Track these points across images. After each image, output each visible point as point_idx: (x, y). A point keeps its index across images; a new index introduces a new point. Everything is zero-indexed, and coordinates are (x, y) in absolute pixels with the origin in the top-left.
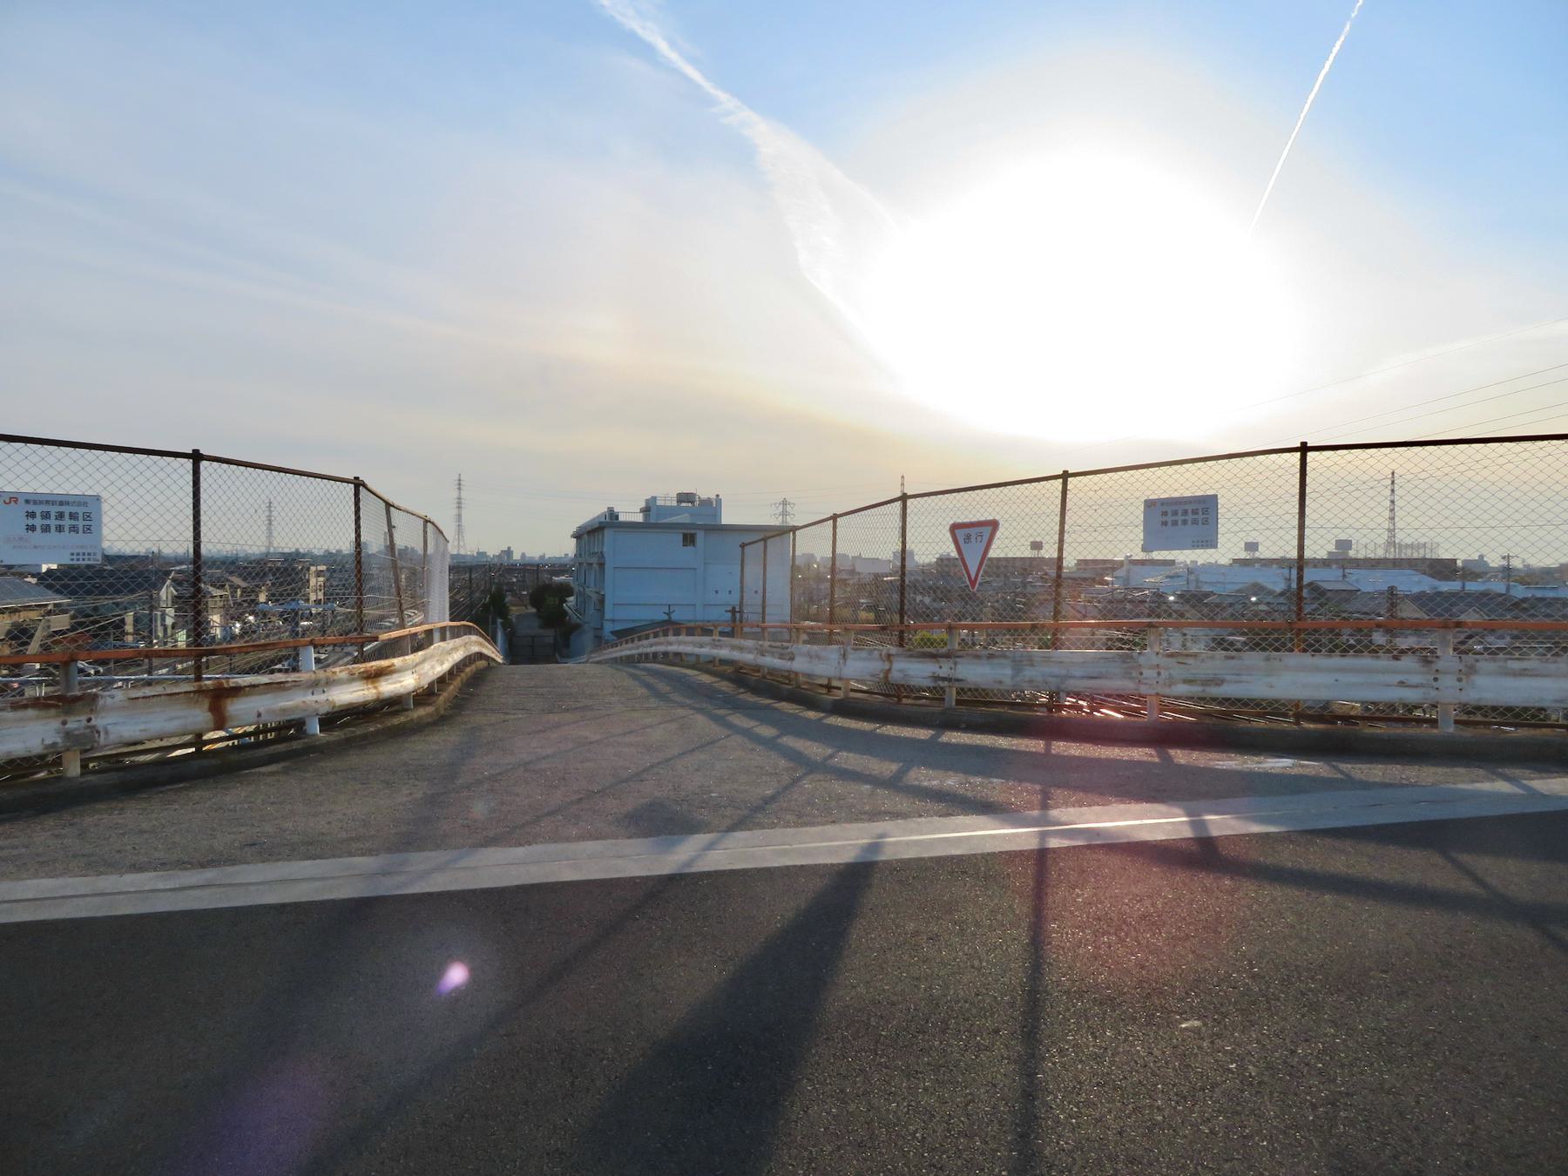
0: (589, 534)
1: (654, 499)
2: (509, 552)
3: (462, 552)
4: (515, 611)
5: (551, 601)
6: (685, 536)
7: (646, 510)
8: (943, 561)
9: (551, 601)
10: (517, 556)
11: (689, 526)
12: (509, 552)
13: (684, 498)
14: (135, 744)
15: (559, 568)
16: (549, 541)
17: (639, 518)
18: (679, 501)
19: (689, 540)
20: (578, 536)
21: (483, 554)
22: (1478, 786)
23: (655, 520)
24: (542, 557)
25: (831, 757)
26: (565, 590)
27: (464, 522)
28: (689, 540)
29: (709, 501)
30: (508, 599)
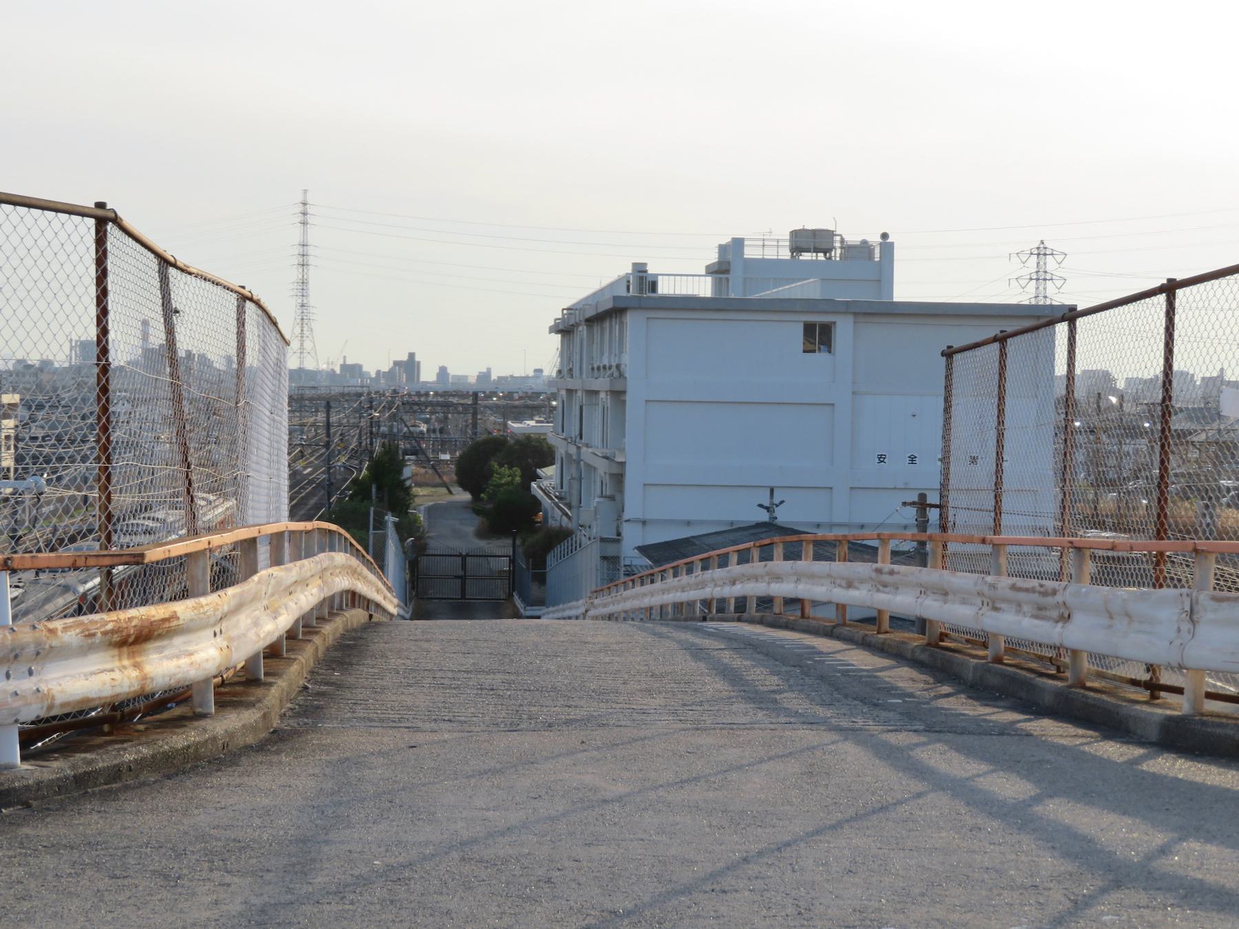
0: (593, 324)
1: (738, 243)
2: (410, 365)
3: (310, 365)
4: (424, 498)
5: (505, 475)
6: (809, 329)
7: (720, 271)
9: (505, 475)
10: (428, 375)
11: (821, 303)
12: (410, 365)
13: (808, 241)
15: (524, 400)
18: (796, 249)
19: (818, 336)
20: (565, 329)
21: (352, 370)
26: (534, 454)
27: (312, 300)
28: (818, 336)
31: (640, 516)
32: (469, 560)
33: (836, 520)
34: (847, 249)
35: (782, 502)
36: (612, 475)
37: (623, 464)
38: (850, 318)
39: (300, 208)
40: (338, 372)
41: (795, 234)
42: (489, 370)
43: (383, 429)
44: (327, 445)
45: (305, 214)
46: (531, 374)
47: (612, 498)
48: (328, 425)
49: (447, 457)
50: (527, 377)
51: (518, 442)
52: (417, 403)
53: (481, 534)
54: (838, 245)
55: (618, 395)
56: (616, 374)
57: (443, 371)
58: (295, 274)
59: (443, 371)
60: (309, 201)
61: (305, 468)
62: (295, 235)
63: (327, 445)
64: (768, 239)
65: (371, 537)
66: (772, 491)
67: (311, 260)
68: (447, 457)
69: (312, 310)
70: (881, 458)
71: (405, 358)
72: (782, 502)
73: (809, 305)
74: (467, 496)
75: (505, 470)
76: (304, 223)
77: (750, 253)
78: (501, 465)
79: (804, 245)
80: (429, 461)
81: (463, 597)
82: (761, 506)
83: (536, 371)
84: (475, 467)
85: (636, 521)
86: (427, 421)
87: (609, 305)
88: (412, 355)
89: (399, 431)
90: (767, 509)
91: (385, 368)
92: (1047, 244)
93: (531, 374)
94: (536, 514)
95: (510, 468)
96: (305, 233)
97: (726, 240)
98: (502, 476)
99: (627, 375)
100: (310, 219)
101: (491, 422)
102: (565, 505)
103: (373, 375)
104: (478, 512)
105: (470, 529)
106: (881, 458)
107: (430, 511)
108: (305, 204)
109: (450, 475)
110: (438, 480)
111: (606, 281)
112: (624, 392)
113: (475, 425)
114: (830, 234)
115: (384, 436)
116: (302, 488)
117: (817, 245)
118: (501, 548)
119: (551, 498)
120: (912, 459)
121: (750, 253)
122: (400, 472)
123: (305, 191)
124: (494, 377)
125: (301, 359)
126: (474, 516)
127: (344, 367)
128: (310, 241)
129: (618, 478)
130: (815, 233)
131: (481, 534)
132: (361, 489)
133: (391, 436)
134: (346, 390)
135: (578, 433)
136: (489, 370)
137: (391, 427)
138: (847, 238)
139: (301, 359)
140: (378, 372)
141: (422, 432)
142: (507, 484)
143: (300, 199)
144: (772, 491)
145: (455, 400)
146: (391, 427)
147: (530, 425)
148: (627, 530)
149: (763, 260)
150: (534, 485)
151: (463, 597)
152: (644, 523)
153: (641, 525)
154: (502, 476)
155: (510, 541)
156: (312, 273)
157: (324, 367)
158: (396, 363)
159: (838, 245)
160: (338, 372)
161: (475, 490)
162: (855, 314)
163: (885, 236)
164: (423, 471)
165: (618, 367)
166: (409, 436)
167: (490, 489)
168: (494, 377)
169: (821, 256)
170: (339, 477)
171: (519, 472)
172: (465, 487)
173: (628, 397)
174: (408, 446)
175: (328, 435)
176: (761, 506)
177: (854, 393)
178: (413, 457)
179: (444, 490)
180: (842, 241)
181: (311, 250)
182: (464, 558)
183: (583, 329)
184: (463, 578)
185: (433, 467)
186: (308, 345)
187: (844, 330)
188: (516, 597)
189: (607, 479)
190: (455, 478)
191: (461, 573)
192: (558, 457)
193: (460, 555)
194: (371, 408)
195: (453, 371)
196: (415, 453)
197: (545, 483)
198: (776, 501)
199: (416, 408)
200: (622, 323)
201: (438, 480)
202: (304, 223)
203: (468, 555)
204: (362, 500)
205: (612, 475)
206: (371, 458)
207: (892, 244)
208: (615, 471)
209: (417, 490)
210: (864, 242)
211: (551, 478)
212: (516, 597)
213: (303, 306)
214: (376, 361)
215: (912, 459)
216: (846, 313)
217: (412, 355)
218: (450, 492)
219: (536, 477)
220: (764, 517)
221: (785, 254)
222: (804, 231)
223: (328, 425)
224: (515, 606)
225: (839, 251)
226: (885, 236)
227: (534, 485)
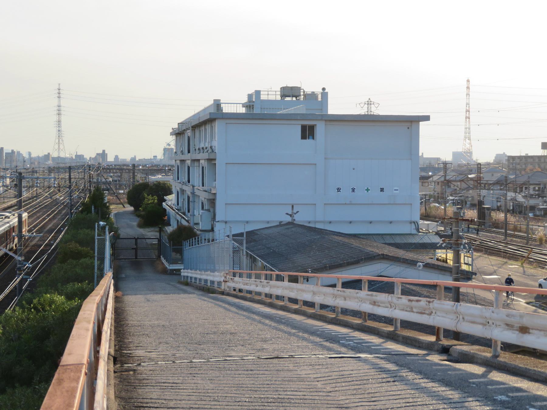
0: (191, 131)
1: (258, 93)
2: (103, 155)
3: (62, 155)
4: (115, 209)
5: (150, 199)
6: (304, 128)
7: (249, 105)
8: (161, 160)
9: (150, 199)
10: (111, 159)
11: (301, 117)
12: (103, 155)
13: (289, 92)
14: (279, 320)
15: (154, 168)
16: (141, 139)
17: (243, 110)
18: (283, 96)
19: (308, 132)
20: (179, 133)
21: (80, 157)
22: (75, 405)
23: (257, 112)
24: (134, 159)
25: (383, 343)
26: (163, 190)
27: (63, 128)
28: (308, 132)
29: (313, 95)
30: (107, 198)
31: (224, 220)
32: (139, 241)
33: (317, 220)
34: (305, 95)
35: (298, 212)
36: (209, 200)
37: (215, 194)
38: (324, 123)
39: (58, 91)
40: (74, 158)
41: (283, 89)
42: (135, 156)
43: (95, 180)
44: (70, 187)
45: (59, 93)
46: (152, 158)
47: (208, 210)
48: (70, 178)
49: (122, 192)
50: (151, 159)
51: (154, 185)
52: (109, 169)
53: (140, 226)
54: (302, 93)
55: (211, 161)
56: (210, 151)
57: (117, 157)
58: (56, 118)
59: (117, 157)
60: (61, 88)
61: (61, 196)
62: (56, 102)
63: (70, 187)
64: (271, 92)
65: (96, 240)
66: (293, 206)
67: (62, 112)
68: (122, 192)
69: (63, 133)
70: (339, 190)
71: (101, 152)
72: (298, 212)
73: (303, 117)
74: (132, 209)
75: (150, 197)
76: (59, 97)
77: (263, 97)
78: (148, 195)
79: (288, 94)
80: (114, 193)
81: (136, 258)
82: (287, 214)
83: (154, 156)
84: (136, 195)
85: (222, 221)
86: (111, 177)
87: (208, 117)
88: (104, 151)
89: (101, 180)
90: (291, 215)
91: (93, 156)
92: (371, 100)
93: (152, 158)
94: (165, 217)
95: (152, 196)
96: (60, 101)
97: (251, 91)
98: (149, 200)
99: (216, 151)
100: (61, 96)
101: (140, 178)
102: (181, 213)
103: (88, 159)
104: (138, 216)
105: (135, 224)
106: (339, 190)
107: (116, 215)
108: (59, 89)
109: (125, 199)
110: (119, 202)
111: (197, 112)
112: (215, 160)
113: (134, 178)
114: (299, 89)
115: (94, 183)
116: (60, 206)
117: (294, 94)
118: (151, 234)
119: (174, 210)
120: (353, 190)
121: (263, 97)
122: (103, 199)
123: (59, 84)
124: (137, 159)
125: (59, 152)
126: (137, 218)
127: (76, 156)
128: (62, 104)
129: (212, 202)
130: (292, 88)
131: (140, 226)
132: (86, 208)
133: (98, 183)
134: (78, 164)
135: (187, 179)
136: (135, 156)
137: (98, 179)
138: (306, 90)
139: (59, 152)
140: (90, 158)
141: (110, 181)
142: (151, 203)
143: (58, 87)
144: (293, 206)
145: (125, 167)
146: (98, 179)
147: (159, 177)
148: (218, 227)
149: (268, 100)
150: (164, 204)
151: (136, 258)
152: (226, 222)
153: (224, 224)
154: (149, 200)
155: (157, 229)
156: (63, 118)
157: (68, 156)
158: (97, 154)
159: (302, 93)
160: (74, 158)
161: (137, 207)
162: (326, 121)
163: (324, 89)
164: (112, 198)
165: (211, 147)
166: (106, 183)
167: (144, 206)
168: (137, 159)
169: (294, 99)
170: (75, 201)
171: (156, 198)
172: (131, 205)
173: (217, 162)
174: (105, 187)
175: (70, 182)
176: (287, 214)
177: (325, 158)
178: (107, 192)
179: (121, 206)
180: (304, 92)
181: (62, 108)
182: (136, 239)
183: (189, 133)
184: (136, 249)
185: (117, 196)
186: (61, 147)
187: (320, 129)
188: (162, 258)
189: (206, 203)
190: (126, 201)
191: (135, 247)
192: (174, 190)
193: (135, 238)
194: (90, 170)
195: (121, 157)
196: (108, 190)
197: (169, 203)
198: (295, 211)
199: (108, 171)
200: (212, 127)
201: (119, 202)
202: (59, 97)
203: (138, 238)
204: (87, 214)
205: (209, 200)
206: (90, 193)
207: (327, 93)
208: (211, 197)
209: (112, 207)
210: (313, 92)
211: (171, 200)
212: (162, 258)
213: (59, 131)
214: (89, 153)
215: (353, 190)
216: (322, 120)
217: (104, 151)
218: (124, 207)
219: (165, 201)
220: (289, 219)
221: (279, 98)
222: (283, 87)
223: (70, 178)
224: (163, 263)
225: (302, 97)
226: (324, 89)
227: (164, 204)
